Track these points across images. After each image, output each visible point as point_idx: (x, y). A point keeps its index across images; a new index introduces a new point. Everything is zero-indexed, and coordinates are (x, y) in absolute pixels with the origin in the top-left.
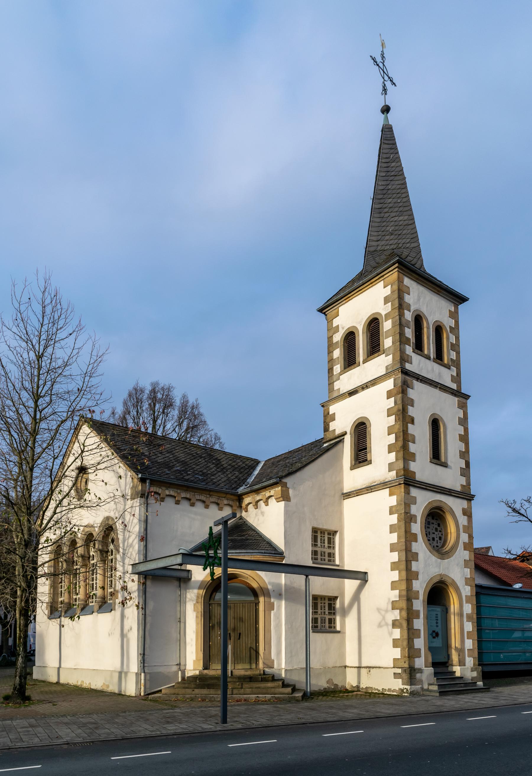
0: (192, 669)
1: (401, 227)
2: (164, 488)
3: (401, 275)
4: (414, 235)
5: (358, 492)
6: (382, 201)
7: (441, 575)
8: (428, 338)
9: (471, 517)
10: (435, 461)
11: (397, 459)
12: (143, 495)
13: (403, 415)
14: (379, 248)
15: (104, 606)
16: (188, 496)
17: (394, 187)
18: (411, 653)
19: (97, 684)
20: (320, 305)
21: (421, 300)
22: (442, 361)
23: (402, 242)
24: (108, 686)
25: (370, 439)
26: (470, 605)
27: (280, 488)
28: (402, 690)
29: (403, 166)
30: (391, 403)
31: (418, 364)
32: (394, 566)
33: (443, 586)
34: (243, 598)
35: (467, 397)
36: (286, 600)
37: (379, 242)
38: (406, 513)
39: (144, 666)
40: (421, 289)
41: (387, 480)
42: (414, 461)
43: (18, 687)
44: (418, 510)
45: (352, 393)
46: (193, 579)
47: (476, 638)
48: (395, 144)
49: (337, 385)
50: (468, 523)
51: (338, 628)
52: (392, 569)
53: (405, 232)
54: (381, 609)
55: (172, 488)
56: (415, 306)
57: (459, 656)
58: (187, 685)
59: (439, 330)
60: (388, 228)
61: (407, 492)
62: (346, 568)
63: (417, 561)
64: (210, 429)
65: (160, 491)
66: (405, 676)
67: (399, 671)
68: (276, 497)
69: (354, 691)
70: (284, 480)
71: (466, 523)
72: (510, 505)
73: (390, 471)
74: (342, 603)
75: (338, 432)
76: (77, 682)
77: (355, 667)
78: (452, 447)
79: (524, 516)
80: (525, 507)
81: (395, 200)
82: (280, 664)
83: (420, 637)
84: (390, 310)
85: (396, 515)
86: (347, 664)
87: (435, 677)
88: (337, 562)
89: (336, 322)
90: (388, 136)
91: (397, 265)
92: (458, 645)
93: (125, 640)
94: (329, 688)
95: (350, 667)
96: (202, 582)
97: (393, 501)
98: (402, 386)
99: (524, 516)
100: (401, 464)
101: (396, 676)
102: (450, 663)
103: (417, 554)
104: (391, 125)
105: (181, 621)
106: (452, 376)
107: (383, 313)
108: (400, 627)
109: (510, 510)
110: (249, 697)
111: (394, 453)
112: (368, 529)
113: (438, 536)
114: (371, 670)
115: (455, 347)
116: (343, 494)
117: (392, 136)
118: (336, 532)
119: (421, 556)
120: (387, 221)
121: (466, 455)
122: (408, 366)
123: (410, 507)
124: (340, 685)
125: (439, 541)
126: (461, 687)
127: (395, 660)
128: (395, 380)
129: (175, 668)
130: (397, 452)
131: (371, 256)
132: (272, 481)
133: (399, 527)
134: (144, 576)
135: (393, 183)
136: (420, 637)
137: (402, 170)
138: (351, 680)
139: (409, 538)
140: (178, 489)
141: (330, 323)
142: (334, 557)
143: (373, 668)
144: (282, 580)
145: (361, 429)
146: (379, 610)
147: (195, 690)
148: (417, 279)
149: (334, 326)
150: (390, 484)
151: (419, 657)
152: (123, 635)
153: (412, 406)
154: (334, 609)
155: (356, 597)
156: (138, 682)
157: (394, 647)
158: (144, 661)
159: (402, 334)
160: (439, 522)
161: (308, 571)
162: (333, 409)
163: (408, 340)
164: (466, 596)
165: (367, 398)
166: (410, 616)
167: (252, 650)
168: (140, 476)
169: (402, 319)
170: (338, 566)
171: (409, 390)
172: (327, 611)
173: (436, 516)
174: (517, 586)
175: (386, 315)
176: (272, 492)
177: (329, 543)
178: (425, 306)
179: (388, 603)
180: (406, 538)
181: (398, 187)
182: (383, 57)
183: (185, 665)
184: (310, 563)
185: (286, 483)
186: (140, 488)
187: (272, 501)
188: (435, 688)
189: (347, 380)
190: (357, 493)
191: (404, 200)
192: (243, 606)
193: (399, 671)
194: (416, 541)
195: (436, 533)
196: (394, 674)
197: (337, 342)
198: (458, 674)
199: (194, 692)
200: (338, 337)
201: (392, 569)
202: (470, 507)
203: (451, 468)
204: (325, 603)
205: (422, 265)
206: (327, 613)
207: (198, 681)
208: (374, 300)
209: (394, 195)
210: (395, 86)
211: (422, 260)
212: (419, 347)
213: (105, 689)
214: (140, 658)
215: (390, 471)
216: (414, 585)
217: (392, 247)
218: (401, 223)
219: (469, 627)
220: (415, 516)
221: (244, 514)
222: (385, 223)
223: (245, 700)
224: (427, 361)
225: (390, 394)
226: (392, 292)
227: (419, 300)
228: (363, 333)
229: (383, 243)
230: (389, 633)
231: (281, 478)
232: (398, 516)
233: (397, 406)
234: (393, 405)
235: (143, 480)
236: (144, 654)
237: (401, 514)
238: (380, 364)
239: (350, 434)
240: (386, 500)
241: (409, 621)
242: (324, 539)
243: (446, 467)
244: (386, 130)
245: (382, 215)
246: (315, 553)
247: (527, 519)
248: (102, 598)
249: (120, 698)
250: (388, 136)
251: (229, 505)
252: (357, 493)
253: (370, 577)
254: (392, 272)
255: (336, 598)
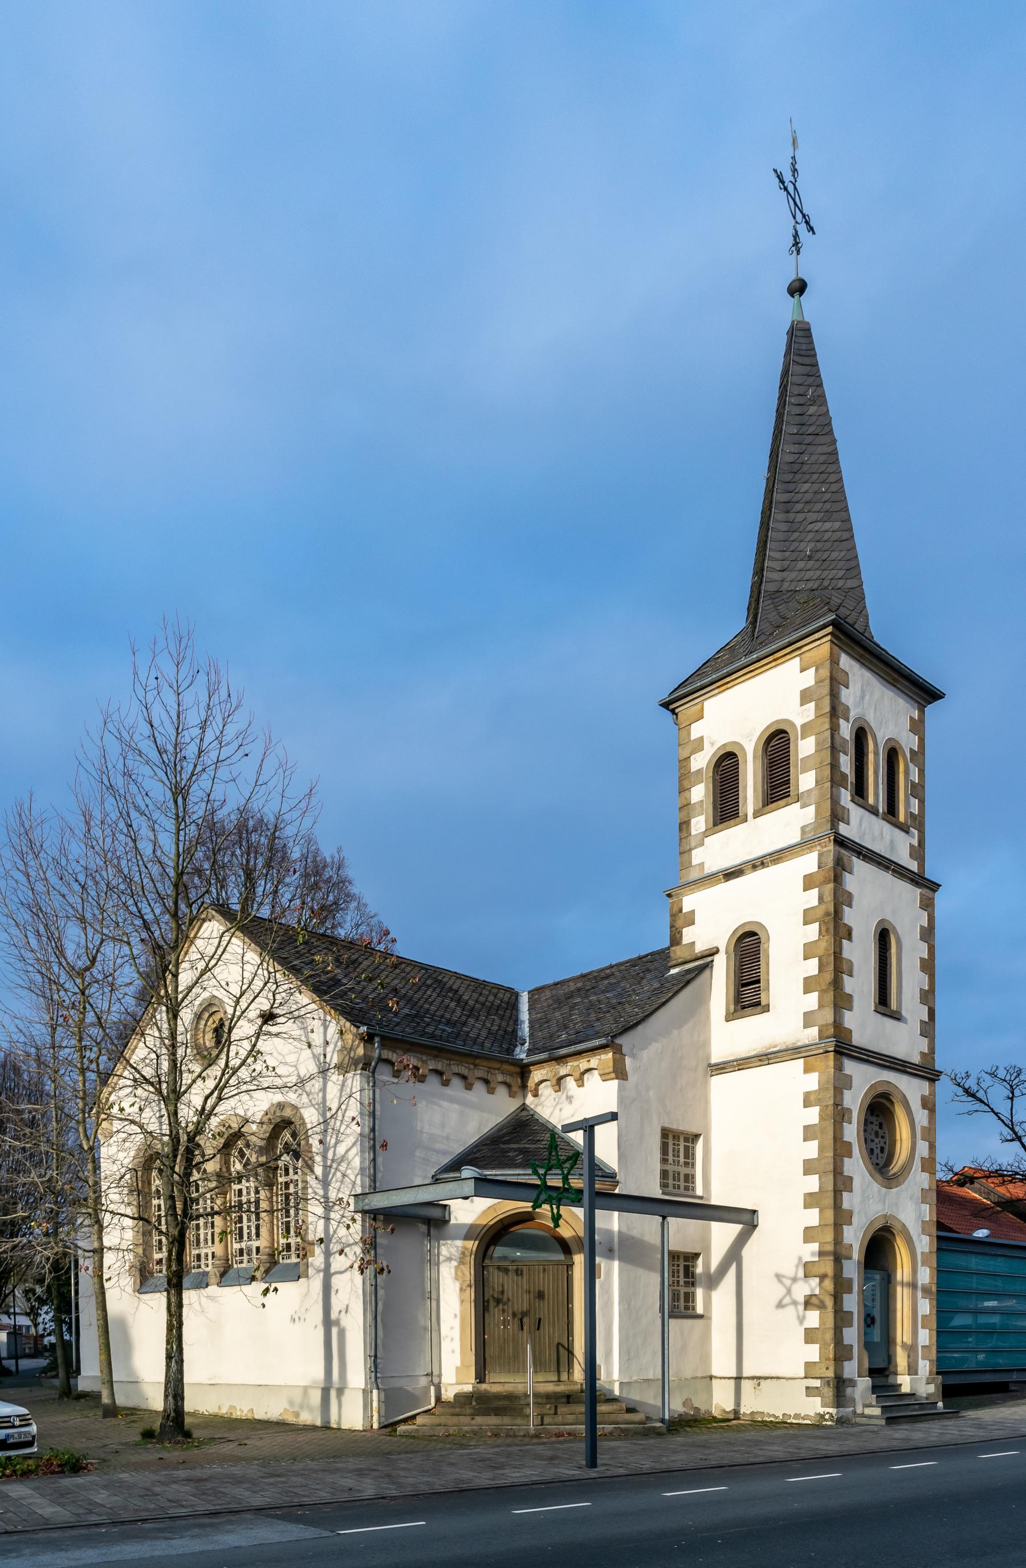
0: (454, 1382)
1: (828, 545)
2: (400, 1052)
3: (836, 648)
4: (852, 564)
5: (742, 1064)
6: (791, 487)
7: (885, 1216)
8: (876, 773)
9: (935, 1111)
10: (882, 1008)
11: (821, 1006)
12: (366, 1065)
13: (835, 925)
14: (786, 586)
15: (275, 1268)
16: (439, 1068)
17: (814, 458)
18: (841, 1353)
19: (271, 1409)
20: (664, 695)
21: (867, 698)
22: (894, 816)
23: (830, 577)
24: (297, 1415)
25: (768, 965)
26: (928, 1269)
27: (610, 1055)
28: (822, 1416)
29: (831, 413)
30: (812, 898)
31: (862, 826)
32: (810, 1200)
33: (887, 1235)
34: (544, 1256)
35: (934, 887)
36: (620, 1259)
37: (785, 574)
38: (836, 1105)
39: (376, 1378)
40: (868, 675)
41: (800, 1044)
42: (850, 1010)
43: (173, 1414)
44: (855, 1100)
45: (731, 874)
46: (453, 1221)
47: (935, 1327)
48: (815, 365)
49: (697, 856)
50: (930, 1123)
51: (700, 1310)
52: (807, 1206)
53: (835, 555)
54: (783, 1276)
55: (414, 1051)
56: (857, 711)
57: (909, 1357)
58: (457, 1410)
59: (892, 755)
60: (803, 545)
61: (839, 1068)
62: (714, 1202)
63: (851, 1191)
64: (372, 914)
65: (393, 1057)
66: (829, 1392)
67: (817, 1383)
68: (602, 1072)
69: (729, 1420)
70: (618, 1041)
71: (925, 1123)
72: (959, 1081)
73: (806, 1025)
74: (707, 1265)
75: (699, 948)
76: (219, 1408)
77: (729, 1378)
78: (909, 981)
79: (982, 1101)
80: (984, 1085)
81: (816, 487)
82: (609, 1373)
83: (851, 1326)
84: (812, 716)
85: (817, 1109)
86: (714, 1373)
87: (873, 1393)
88: (699, 1192)
89: (696, 730)
90: (800, 341)
91: (830, 629)
92: (908, 1339)
93: (335, 1331)
94: (686, 1414)
95: (720, 1378)
96: (472, 1227)
97: (812, 1082)
98: (835, 869)
99: (982, 1101)
100: (828, 1016)
101: (810, 1391)
102: (892, 1369)
103: (851, 1179)
104: (808, 323)
105: (433, 1296)
106: (911, 846)
107: (799, 722)
108: (821, 1306)
109: (960, 1091)
110: (575, 1429)
111: (816, 994)
112: (760, 1131)
113: (879, 1146)
114: (762, 1382)
115: (917, 790)
116: (710, 1065)
117: (810, 347)
118: (697, 1136)
119: (856, 1184)
120: (801, 529)
121: (930, 997)
122: (843, 829)
123: (842, 1094)
124: (703, 1409)
125: (880, 1155)
126: (915, 1410)
127: (808, 1365)
128: (820, 855)
129: (423, 1381)
130: (822, 993)
131: (770, 602)
132: (597, 1042)
133: (823, 1131)
134: (372, 1216)
135: (811, 449)
136: (851, 1326)
137: (829, 424)
138: (721, 1400)
139: (840, 1149)
140: (422, 1053)
141: (684, 732)
142: (693, 1182)
143: (766, 1378)
144: (613, 1224)
145: (749, 946)
146: (779, 1277)
147: (477, 1418)
148: (861, 656)
149: (692, 738)
150: (806, 1051)
151: (850, 1359)
152: (328, 1323)
153: (850, 906)
154: (693, 1275)
155: (734, 1255)
156: (367, 1405)
157: (806, 1342)
158: (376, 1367)
159: (834, 766)
160: (881, 1119)
161: (666, 1209)
162: (689, 902)
163: (844, 776)
164: (922, 1253)
165: (757, 885)
166: (841, 1286)
167: (561, 1348)
168: (364, 1029)
169: (836, 736)
170: (701, 1198)
171: (847, 876)
172: (682, 1280)
173: (880, 1109)
174: (981, 1233)
175: (803, 726)
176: (594, 1062)
177: (686, 1156)
178: (872, 711)
179: (797, 1266)
180: (835, 1150)
181: (823, 458)
182: (795, 170)
183: (440, 1376)
184: (657, 1193)
185: (621, 1046)
186: (361, 1051)
187: (593, 1080)
188: (877, 1411)
189: (718, 849)
190: (738, 1065)
191: (834, 487)
192: (544, 1270)
193: (817, 1383)
194: (850, 1156)
195: (877, 1140)
196: (807, 1388)
197: (699, 771)
198: (906, 1389)
199: (473, 1422)
200: (701, 761)
201: (807, 1206)
202: (933, 1093)
203: (906, 1023)
204: (678, 1266)
205: (867, 626)
206: (682, 1283)
207: (474, 1403)
208: (777, 694)
209: (815, 476)
210: (814, 233)
211: (867, 616)
212: (860, 791)
213: (290, 1419)
214: (370, 1362)
215: (806, 1025)
216: (845, 1235)
217: (810, 585)
218: (827, 536)
219: (925, 1307)
220: (850, 1111)
221: (530, 1100)
222: (796, 535)
223: (569, 1434)
224: (873, 817)
225: (809, 882)
226: (819, 682)
227: (863, 697)
228: (754, 757)
229: (793, 575)
230: (798, 1317)
231: (614, 1037)
232: (821, 1110)
233: (823, 907)
234: (815, 902)
235: (368, 1039)
236: (376, 1356)
237: (827, 1106)
238: (790, 822)
239: (727, 953)
240: (798, 1079)
241: (837, 1298)
242: (678, 1145)
243: (898, 1019)
244: (799, 333)
245: (791, 516)
246: (664, 1174)
247: (986, 1108)
248: (269, 1255)
249: (339, 1433)
250: (800, 341)
251: (505, 1083)
252: (738, 1065)
253: (762, 1220)
254: (819, 642)
255: (697, 1255)
